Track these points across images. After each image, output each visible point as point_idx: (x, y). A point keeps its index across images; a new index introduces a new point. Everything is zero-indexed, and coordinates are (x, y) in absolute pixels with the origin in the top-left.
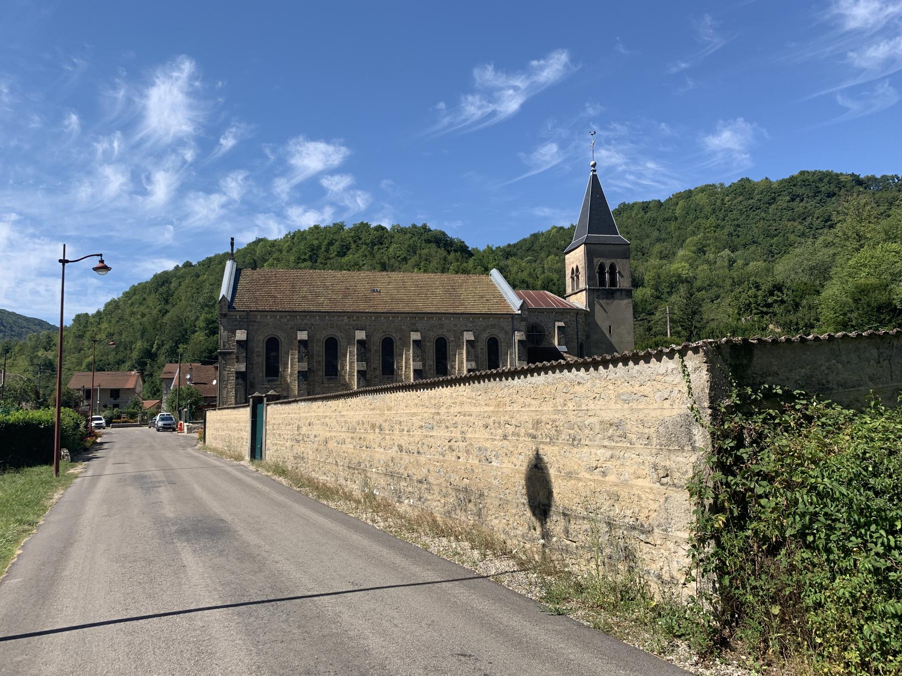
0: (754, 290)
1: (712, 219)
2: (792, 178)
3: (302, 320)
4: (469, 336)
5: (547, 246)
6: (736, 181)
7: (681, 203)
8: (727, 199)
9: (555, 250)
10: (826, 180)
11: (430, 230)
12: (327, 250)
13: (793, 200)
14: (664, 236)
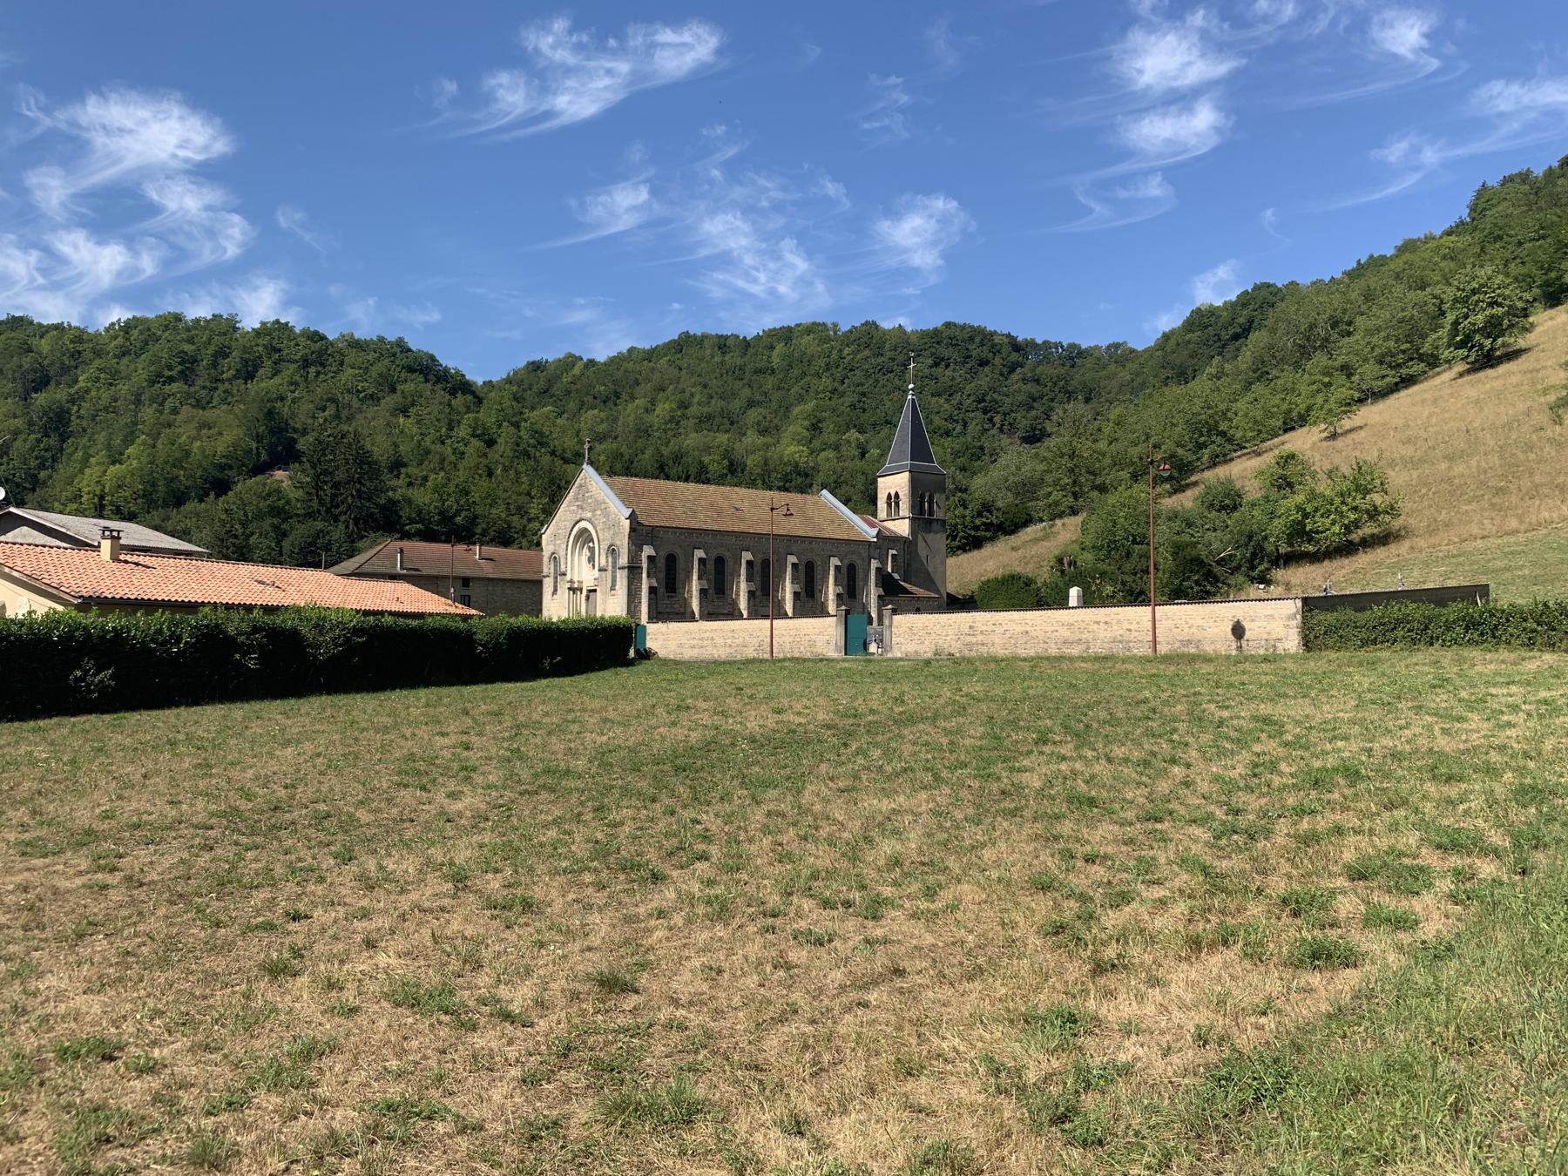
1: (826, 381)
4: (699, 554)
5: (577, 391)
7: (780, 347)
8: (847, 350)
9: (590, 398)
10: (978, 340)
12: (214, 365)
13: (936, 364)
14: (758, 397)
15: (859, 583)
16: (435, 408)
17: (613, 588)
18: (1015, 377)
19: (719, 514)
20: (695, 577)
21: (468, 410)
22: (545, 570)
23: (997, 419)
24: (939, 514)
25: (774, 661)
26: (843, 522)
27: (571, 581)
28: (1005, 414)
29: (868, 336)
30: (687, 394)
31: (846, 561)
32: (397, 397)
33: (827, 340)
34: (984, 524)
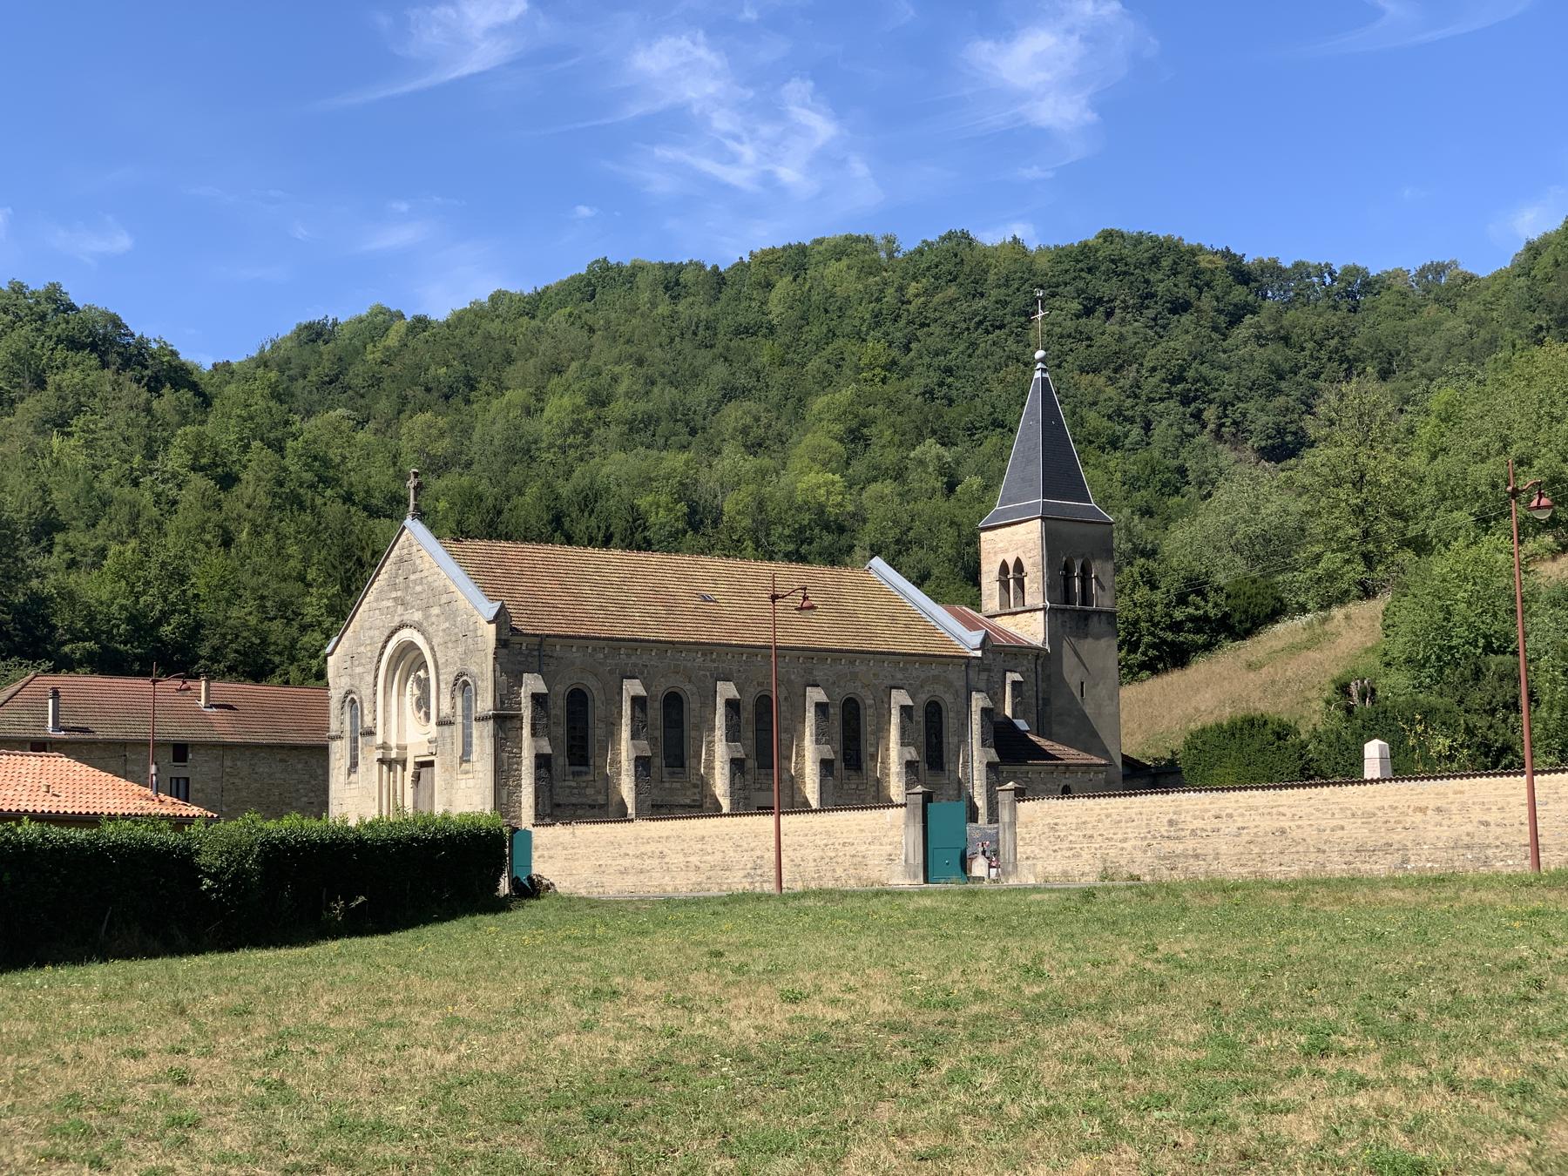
0: (1146, 590)
1: (874, 348)
2: (1085, 250)
3: (628, 656)
4: (633, 688)
5: (394, 378)
6: (933, 238)
7: (783, 285)
9: (419, 391)
10: (1166, 263)
11: (72, 307)
13: (1088, 312)
14: (742, 380)
15: (950, 739)
16: (121, 417)
17: (465, 757)
18: (1242, 331)
19: (670, 610)
20: (625, 733)
21: (185, 420)
22: (334, 726)
23: (1210, 414)
24: (1102, 600)
25: (783, 896)
26: (916, 620)
27: (385, 747)
28: (1224, 405)
29: (955, 262)
30: (605, 379)
31: (924, 697)
32: (48, 398)
33: (873, 269)
34: (1191, 618)
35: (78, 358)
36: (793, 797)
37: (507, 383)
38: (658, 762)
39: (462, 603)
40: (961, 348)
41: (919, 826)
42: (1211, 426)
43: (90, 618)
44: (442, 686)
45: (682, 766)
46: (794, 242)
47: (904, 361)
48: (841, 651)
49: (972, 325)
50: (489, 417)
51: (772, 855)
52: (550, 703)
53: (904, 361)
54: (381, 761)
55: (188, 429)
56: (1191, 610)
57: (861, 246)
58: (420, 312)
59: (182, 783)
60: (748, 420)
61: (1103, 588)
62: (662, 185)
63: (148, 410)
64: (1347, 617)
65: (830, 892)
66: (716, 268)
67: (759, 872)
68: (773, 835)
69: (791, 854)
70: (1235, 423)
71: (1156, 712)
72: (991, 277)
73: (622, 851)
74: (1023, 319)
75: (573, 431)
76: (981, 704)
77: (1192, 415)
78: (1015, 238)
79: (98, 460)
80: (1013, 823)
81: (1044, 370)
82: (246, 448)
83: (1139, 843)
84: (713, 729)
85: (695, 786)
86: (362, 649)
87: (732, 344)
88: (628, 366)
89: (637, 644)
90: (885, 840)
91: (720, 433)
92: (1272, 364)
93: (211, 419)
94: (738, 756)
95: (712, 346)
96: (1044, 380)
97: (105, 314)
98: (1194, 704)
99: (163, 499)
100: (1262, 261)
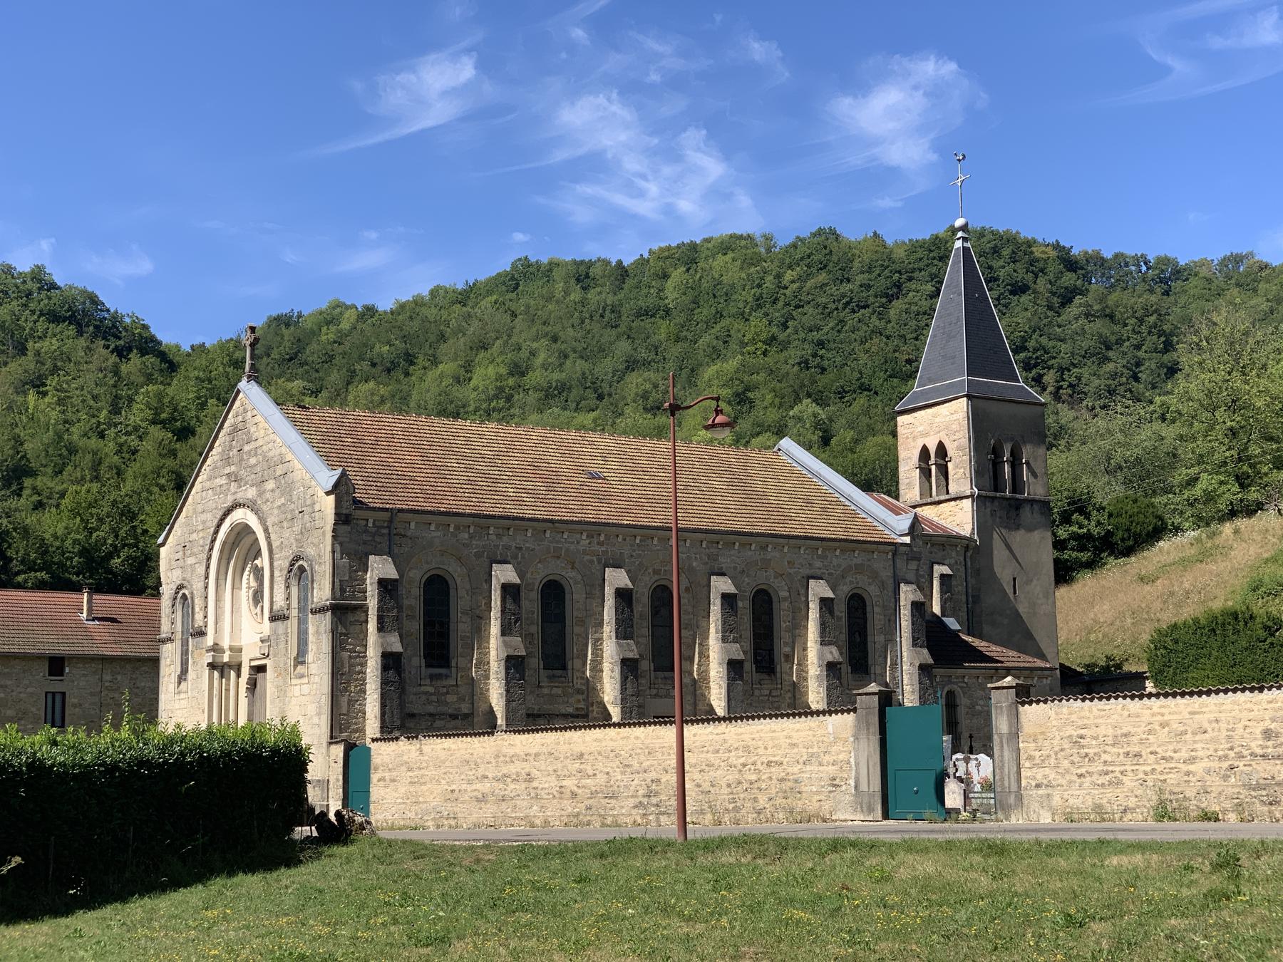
4: (504, 574)
6: (805, 234)
7: (677, 274)
9: (365, 366)
10: (1006, 252)
11: (53, 286)
14: (643, 354)
15: (876, 638)
16: (90, 378)
17: (300, 660)
18: (1074, 309)
19: (551, 486)
20: (495, 629)
21: (149, 379)
22: (165, 628)
23: (1050, 378)
24: (1034, 488)
25: (687, 846)
26: (831, 503)
27: (216, 649)
28: (1062, 370)
29: (823, 253)
30: (524, 354)
31: (845, 589)
32: (28, 362)
33: (756, 260)
34: (1075, 537)
35: (58, 329)
36: (695, 704)
37: (442, 358)
38: (535, 662)
39: (299, 474)
40: (831, 325)
41: (875, 739)
42: (1050, 389)
43: (43, 549)
44: (277, 573)
45: (564, 668)
46: (687, 241)
47: (782, 337)
48: (751, 534)
49: (840, 306)
50: (425, 385)
51: (673, 778)
52: (402, 591)
53: (782, 337)
54: (212, 666)
55: (150, 387)
56: (1074, 529)
57: (743, 243)
58: (369, 302)
59: (58, 698)
60: (648, 386)
61: (1035, 475)
62: (582, 216)
63: (116, 372)
64: (1236, 532)
65: (761, 840)
66: (620, 263)
67: (654, 800)
68: (674, 751)
69: (697, 776)
70: (1071, 385)
71: (1102, 609)
72: (856, 265)
73: (480, 772)
74: (884, 300)
75: (496, 397)
76: (911, 597)
77: (1033, 379)
78: (875, 233)
79: (70, 416)
80: (1015, 735)
81: (965, 239)
82: (203, 406)
83: (1215, 764)
84: (601, 624)
85: (579, 692)
86: (194, 536)
87: (633, 325)
88: (544, 342)
89: (508, 522)
90: (826, 758)
91: (624, 398)
92: (1101, 336)
93: (175, 382)
94: (630, 655)
95: (616, 326)
96: (966, 250)
97: (84, 292)
98: (1092, 615)
99: (125, 448)
100: (1086, 253)
